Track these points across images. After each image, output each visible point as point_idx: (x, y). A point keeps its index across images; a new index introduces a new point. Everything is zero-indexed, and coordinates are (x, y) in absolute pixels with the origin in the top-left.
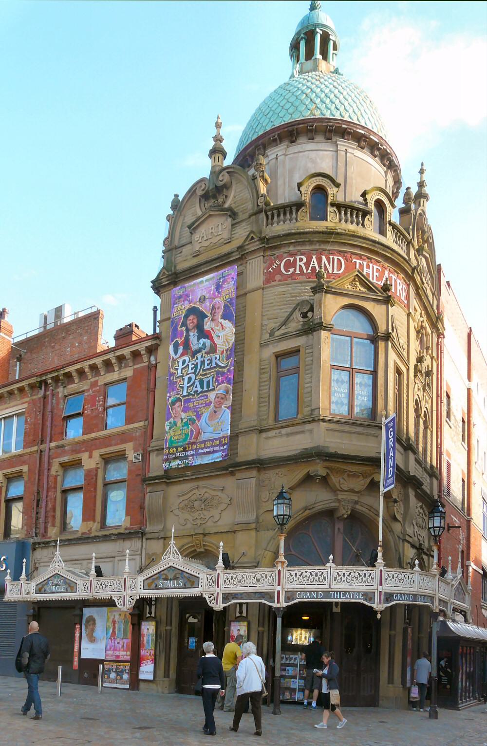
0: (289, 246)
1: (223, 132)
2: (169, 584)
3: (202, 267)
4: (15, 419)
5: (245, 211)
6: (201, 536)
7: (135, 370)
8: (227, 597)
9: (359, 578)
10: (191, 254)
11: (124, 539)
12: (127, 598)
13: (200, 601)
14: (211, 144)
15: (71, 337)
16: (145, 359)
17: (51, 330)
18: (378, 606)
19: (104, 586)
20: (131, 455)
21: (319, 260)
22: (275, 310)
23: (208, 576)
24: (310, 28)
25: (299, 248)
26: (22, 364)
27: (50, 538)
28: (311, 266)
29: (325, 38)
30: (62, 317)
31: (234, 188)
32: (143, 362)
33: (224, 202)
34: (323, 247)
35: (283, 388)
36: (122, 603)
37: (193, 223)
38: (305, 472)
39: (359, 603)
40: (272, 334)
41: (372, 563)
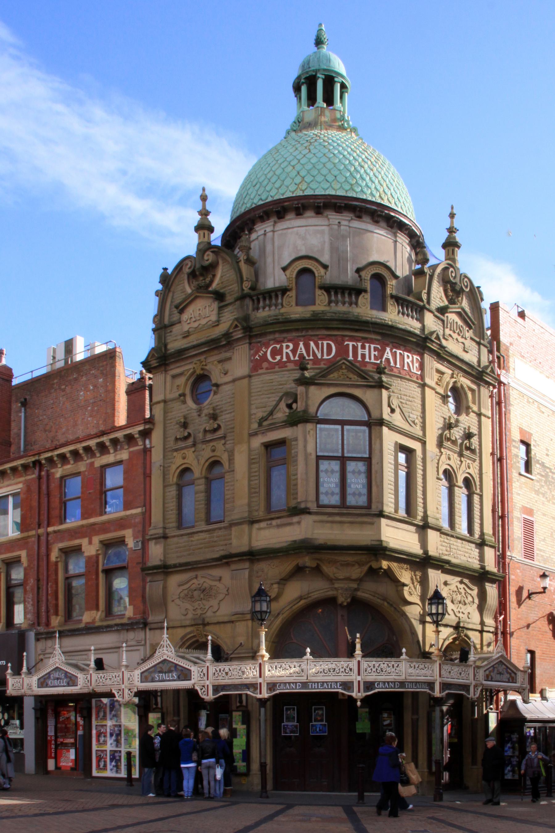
2: (164, 676)
3: (190, 351)
5: (232, 293)
6: (201, 626)
7: (130, 453)
8: (217, 689)
10: (181, 335)
11: (127, 630)
12: (126, 691)
13: (192, 693)
14: (196, 218)
15: (84, 379)
16: (140, 443)
18: (357, 694)
19: (104, 679)
20: (130, 542)
23: (199, 669)
25: (285, 335)
26: (28, 410)
27: (53, 628)
28: (298, 352)
29: (329, 81)
30: (74, 353)
33: (212, 282)
34: (310, 333)
37: (181, 304)
38: (294, 564)
40: (260, 424)
41: (351, 654)
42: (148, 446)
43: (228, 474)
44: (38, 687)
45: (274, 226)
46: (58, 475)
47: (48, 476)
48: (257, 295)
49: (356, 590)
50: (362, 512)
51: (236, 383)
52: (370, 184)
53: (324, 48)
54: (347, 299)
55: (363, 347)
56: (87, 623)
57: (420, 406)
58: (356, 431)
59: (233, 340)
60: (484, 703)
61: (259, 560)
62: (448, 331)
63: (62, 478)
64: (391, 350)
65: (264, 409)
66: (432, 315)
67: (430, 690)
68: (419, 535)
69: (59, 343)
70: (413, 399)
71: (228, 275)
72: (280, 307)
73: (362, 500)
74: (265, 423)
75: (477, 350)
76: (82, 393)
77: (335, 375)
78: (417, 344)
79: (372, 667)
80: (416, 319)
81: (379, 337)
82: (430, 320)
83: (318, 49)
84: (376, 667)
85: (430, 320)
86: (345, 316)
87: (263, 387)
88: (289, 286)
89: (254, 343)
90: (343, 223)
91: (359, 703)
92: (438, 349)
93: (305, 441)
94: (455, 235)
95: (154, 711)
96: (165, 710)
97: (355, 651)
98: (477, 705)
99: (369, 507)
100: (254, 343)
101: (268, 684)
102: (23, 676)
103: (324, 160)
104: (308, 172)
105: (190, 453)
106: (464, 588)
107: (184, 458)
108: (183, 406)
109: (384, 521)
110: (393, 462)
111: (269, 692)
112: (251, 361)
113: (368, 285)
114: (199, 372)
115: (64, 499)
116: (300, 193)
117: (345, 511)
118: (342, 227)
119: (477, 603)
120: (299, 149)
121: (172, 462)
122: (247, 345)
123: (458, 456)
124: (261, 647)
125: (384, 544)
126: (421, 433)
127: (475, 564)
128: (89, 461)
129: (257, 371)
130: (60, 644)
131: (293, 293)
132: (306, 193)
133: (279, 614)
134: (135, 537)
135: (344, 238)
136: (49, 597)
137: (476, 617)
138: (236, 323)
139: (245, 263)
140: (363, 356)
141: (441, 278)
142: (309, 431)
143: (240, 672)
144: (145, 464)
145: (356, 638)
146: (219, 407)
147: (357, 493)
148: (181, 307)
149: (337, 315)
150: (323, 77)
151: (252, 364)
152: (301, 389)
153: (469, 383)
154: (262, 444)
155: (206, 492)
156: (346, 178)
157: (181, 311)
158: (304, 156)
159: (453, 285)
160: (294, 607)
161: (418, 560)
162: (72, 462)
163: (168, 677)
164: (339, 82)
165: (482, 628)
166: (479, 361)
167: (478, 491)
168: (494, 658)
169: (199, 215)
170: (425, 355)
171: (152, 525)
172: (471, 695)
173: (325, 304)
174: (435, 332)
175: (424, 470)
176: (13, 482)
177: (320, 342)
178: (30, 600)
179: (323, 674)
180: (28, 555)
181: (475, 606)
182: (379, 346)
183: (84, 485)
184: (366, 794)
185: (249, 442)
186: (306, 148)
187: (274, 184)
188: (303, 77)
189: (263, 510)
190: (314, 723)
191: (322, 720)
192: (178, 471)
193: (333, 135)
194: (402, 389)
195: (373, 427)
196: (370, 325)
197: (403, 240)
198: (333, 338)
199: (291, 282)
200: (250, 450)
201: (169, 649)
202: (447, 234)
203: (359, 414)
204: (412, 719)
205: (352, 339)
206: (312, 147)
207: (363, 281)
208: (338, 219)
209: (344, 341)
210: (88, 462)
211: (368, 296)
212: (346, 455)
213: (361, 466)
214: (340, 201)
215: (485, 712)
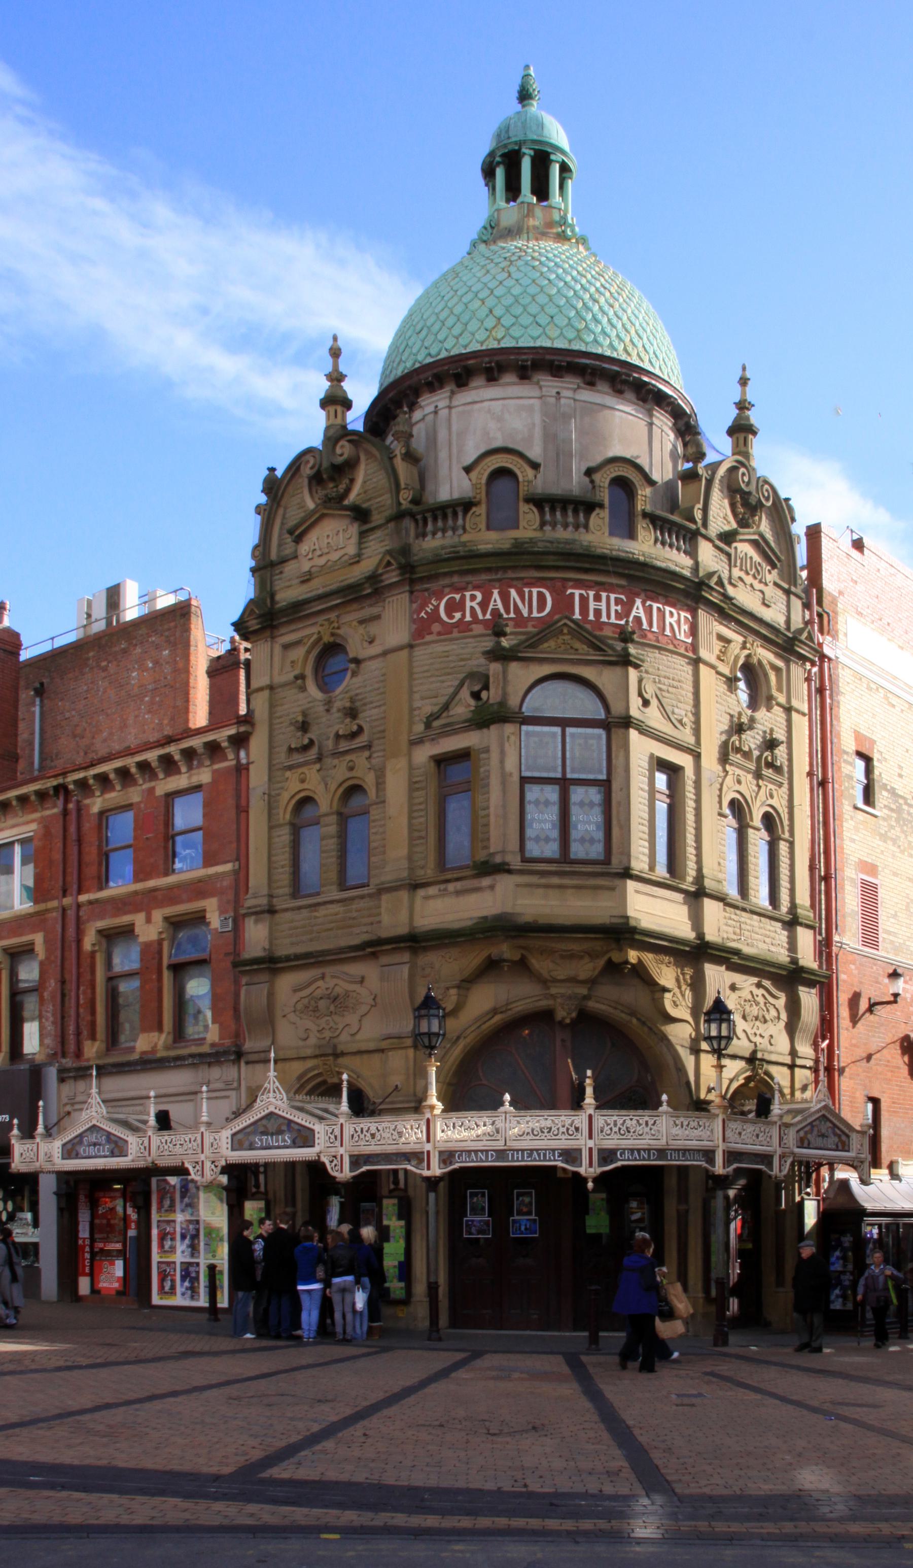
3: (313, 604)
6: (331, 1058)
7: (214, 772)
10: (298, 578)
11: (210, 1064)
12: (208, 1165)
13: (316, 1168)
14: (323, 386)
15: (138, 650)
16: (231, 756)
17: (99, 637)
18: (588, 1169)
19: (171, 1146)
20: (215, 920)
21: (505, 598)
22: (432, 683)
24: (510, 147)
25: (469, 578)
26: (46, 701)
27: (88, 1060)
28: (491, 607)
29: (542, 160)
30: (121, 608)
33: (348, 490)
34: (510, 574)
35: (450, 816)
36: (200, 1173)
37: (297, 526)
38: (485, 954)
40: (428, 725)
41: (577, 1103)
42: (244, 761)
43: (375, 807)
44: (63, 1158)
45: (451, 398)
46: (95, 809)
48: (423, 512)
49: (586, 998)
50: (596, 870)
51: (389, 656)
52: (608, 329)
53: (533, 105)
54: (571, 519)
55: (598, 598)
57: (690, 696)
60: (797, 1185)
61: (426, 949)
62: (736, 572)
63: (102, 813)
64: (643, 603)
65: (434, 700)
66: (710, 545)
67: (707, 1162)
69: (97, 591)
70: (679, 684)
72: (460, 531)
73: (596, 851)
74: (436, 724)
75: (785, 603)
76: (134, 674)
78: (686, 594)
79: (612, 1125)
80: (685, 552)
81: (623, 582)
82: (707, 554)
83: (523, 106)
84: (619, 1125)
85: (707, 554)
87: (432, 664)
88: (475, 498)
90: (565, 393)
92: (721, 601)
93: (502, 753)
94: (749, 413)
95: (253, 1197)
96: (271, 1196)
97: (583, 1099)
98: (784, 1188)
99: (607, 861)
100: (417, 591)
101: (441, 1153)
102: (38, 1140)
103: (533, 290)
104: (507, 311)
105: (312, 773)
106: (763, 995)
107: (303, 781)
108: (302, 695)
109: (631, 885)
110: (647, 788)
111: (442, 1165)
112: (414, 621)
113: (605, 496)
114: (327, 639)
115: (105, 849)
117: (567, 868)
118: (563, 401)
121: (282, 788)
122: (407, 594)
123: (754, 778)
124: (429, 1093)
125: (632, 923)
126: (691, 740)
127: (782, 955)
128: (146, 786)
129: (423, 638)
130: (99, 1087)
131: (482, 510)
132: (503, 345)
133: (458, 1038)
135: (566, 417)
136: (81, 1010)
138: (388, 558)
139: (403, 459)
140: (598, 612)
142: (508, 737)
143: (395, 1133)
148: (297, 533)
149: (555, 545)
150: (532, 153)
152: (495, 668)
153: (771, 657)
156: (569, 319)
157: (298, 539)
158: (501, 283)
159: (745, 495)
160: (484, 1027)
161: (687, 949)
162: (118, 787)
163: (277, 1141)
164: (558, 162)
165: (793, 1060)
166: (788, 622)
167: (786, 835)
168: (813, 1110)
169: (328, 380)
170: (700, 611)
171: (250, 891)
173: (534, 527)
174: (715, 573)
175: (698, 801)
176: (21, 820)
177: (526, 590)
178: (49, 1015)
179: (532, 1137)
180: (46, 941)
181: (782, 1024)
182: (623, 597)
183: (139, 826)
184: (601, 1334)
185: (409, 755)
186: (503, 269)
187: (450, 329)
188: (499, 153)
189: (432, 866)
191: (530, 1213)
192: (293, 802)
194: (661, 667)
196: (609, 562)
198: (549, 583)
199: (478, 491)
200: (411, 768)
201: (278, 1095)
202: (735, 412)
203: (591, 708)
204: (678, 1211)
205: (579, 584)
206: (512, 269)
207: (597, 488)
208: (557, 387)
209: (566, 589)
210: (144, 787)
211: (605, 514)
212: (569, 776)
213: (594, 795)
214: (560, 358)
215: (798, 1199)
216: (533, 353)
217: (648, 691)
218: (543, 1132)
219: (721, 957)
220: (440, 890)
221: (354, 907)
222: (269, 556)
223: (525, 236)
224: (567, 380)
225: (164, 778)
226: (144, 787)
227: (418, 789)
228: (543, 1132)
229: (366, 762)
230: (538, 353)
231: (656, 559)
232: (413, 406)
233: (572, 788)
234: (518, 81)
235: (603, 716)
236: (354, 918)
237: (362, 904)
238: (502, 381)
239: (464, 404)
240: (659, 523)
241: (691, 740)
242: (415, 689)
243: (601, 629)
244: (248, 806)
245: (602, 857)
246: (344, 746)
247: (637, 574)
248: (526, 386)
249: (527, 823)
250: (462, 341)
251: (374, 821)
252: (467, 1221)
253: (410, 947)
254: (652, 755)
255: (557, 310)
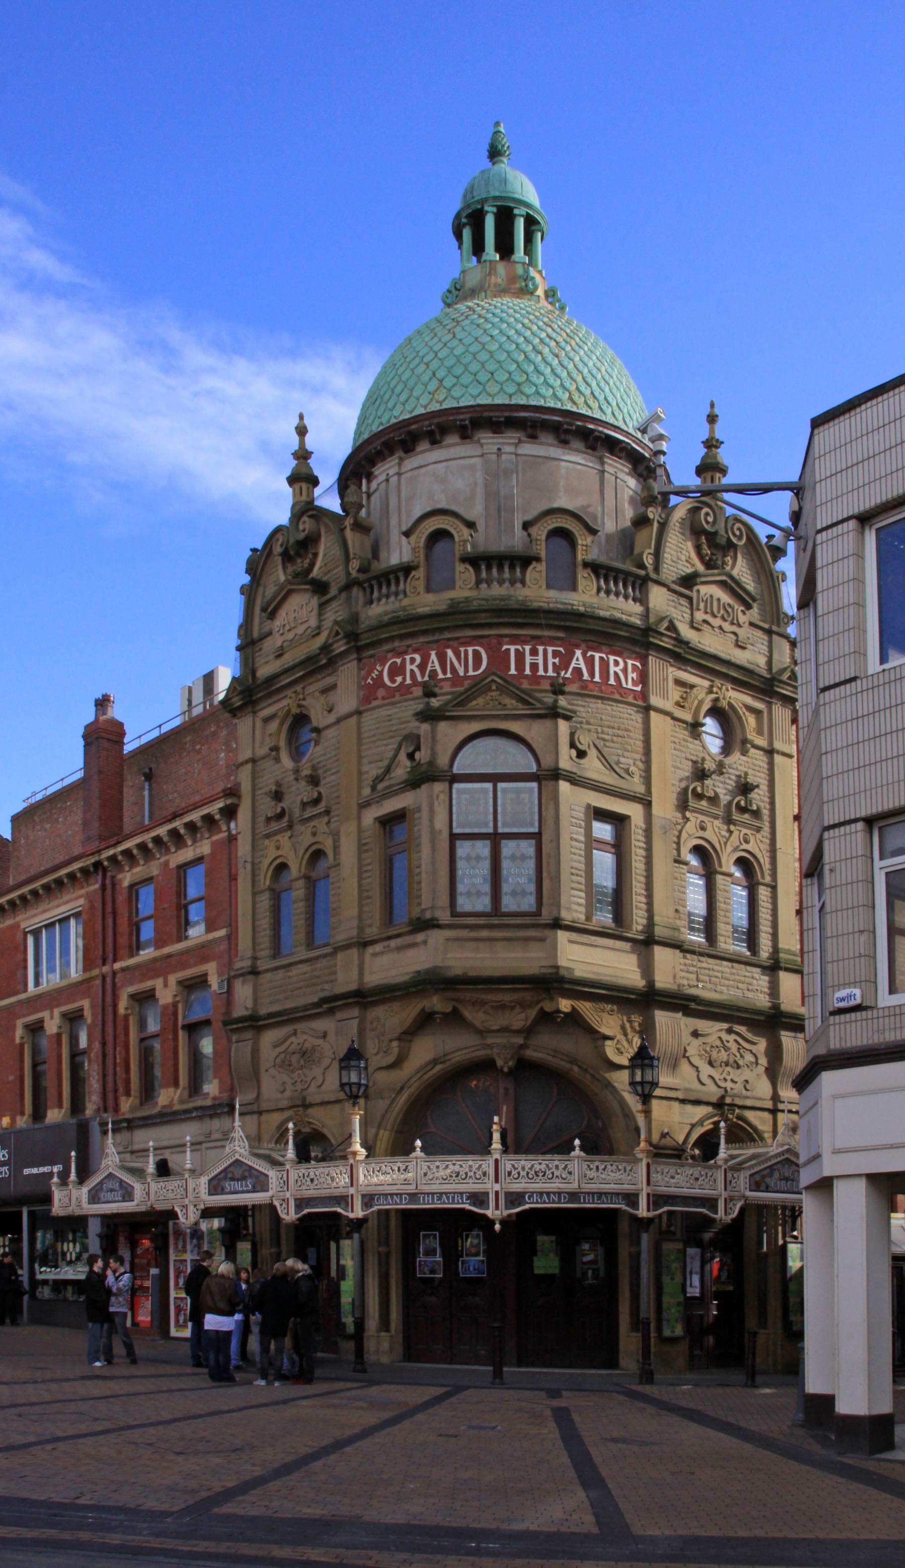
0: (393, 642)
1: (310, 442)
2: (237, 1186)
3: (282, 677)
4: (73, 922)
6: (301, 1109)
7: (213, 844)
9: (513, 1173)
12: (191, 1208)
15: (224, 733)
16: (224, 828)
20: (214, 982)
21: (442, 659)
22: (378, 747)
25: (409, 642)
26: (154, 785)
27: (123, 1114)
28: (429, 668)
29: (505, 217)
30: (215, 693)
31: (323, 539)
32: (221, 831)
33: (312, 565)
34: (447, 635)
39: (463, 1210)
40: (374, 788)
42: (234, 832)
43: (333, 870)
44: (89, 1203)
45: (400, 465)
46: (126, 883)
47: (114, 885)
48: (369, 580)
49: (522, 1047)
50: (524, 922)
51: (342, 723)
52: (551, 380)
53: (502, 162)
54: (507, 575)
55: (534, 652)
56: (164, 1107)
57: (640, 744)
58: (518, 791)
59: (336, 655)
60: (780, 1228)
61: (374, 1004)
62: (699, 616)
63: (131, 886)
64: (584, 654)
65: (380, 764)
66: (664, 590)
67: (628, 1205)
68: (639, 955)
69: (195, 677)
70: (625, 733)
71: (332, 552)
72: (401, 596)
73: (528, 903)
74: (380, 786)
75: (766, 643)
76: (222, 755)
77: (480, 701)
78: (633, 641)
79: (520, 1169)
80: (635, 600)
81: (561, 634)
82: (658, 598)
83: (494, 164)
84: (527, 1169)
85: (658, 598)
86: (503, 603)
87: (377, 728)
88: (413, 562)
89: (365, 658)
90: (507, 449)
91: (497, 1227)
92: (674, 646)
93: (432, 812)
94: (718, 450)
95: (244, 1238)
96: (258, 1238)
97: (490, 1144)
98: (766, 1231)
99: (538, 913)
100: (365, 658)
101: (363, 1196)
102: (71, 1187)
103: (474, 348)
104: (449, 372)
105: (284, 839)
106: (736, 1041)
107: (278, 848)
108: (277, 766)
109: (562, 936)
110: (582, 838)
112: (360, 687)
113: (542, 550)
114: (295, 710)
115: (135, 919)
116: (435, 407)
117: (496, 921)
118: (504, 457)
119: (766, 1064)
120: (439, 335)
121: (263, 856)
122: (355, 662)
123: (723, 823)
124: (353, 1140)
125: (562, 972)
126: (641, 789)
127: (762, 1001)
128: (163, 860)
129: (370, 703)
130: (113, 1138)
131: (420, 573)
132: (444, 406)
133: (402, 1088)
134: (220, 974)
135: (507, 473)
136: (118, 1069)
137: (763, 1088)
138: (337, 628)
139: (352, 530)
140: (534, 667)
141: (688, 525)
142: (438, 796)
143: (329, 1178)
144: (230, 860)
145: (493, 1123)
146: (322, 764)
147: (474, 891)
148: (269, 610)
149: (489, 603)
150: (495, 210)
151: (362, 693)
152: (424, 728)
153: (749, 700)
154: (376, 819)
155: (307, 900)
156: (510, 374)
157: (272, 615)
158: (445, 344)
159: (712, 537)
160: (426, 1077)
161: (633, 997)
162: (142, 862)
163: (242, 1186)
164: (522, 216)
165: (775, 1104)
166: (770, 663)
167: (768, 879)
168: (772, 1154)
169: (295, 459)
170: (650, 658)
171: (240, 954)
172: (720, 1214)
173: (469, 586)
174: (667, 616)
175: (649, 850)
176: (74, 895)
177: (462, 649)
178: (95, 1074)
179: (527, 1180)
180: (93, 1007)
181: (761, 1070)
182: (561, 649)
183: (158, 898)
184: (505, 1369)
185: (359, 818)
186: (449, 331)
187: (398, 396)
188: (464, 215)
189: (378, 925)
190: (465, 1258)
191: (477, 1254)
192: (272, 868)
193: (522, 306)
194: (604, 717)
195: (543, 783)
196: (542, 615)
197: (616, 467)
198: (484, 641)
199: (417, 555)
200: (360, 830)
201: (242, 1144)
204: (630, 1253)
205: (515, 639)
206: (458, 330)
207: (534, 543)
208: (498, 444)
209: (501, 645)
210: (162, 860)
211: (542, 567)
212: (500, 830)
213: (527, 848)
214: (497, 414)
215: (781, 1242)
216: (471, 412)
217: (582, 741)
218: (538, 1176)
219: (666, 1002)
220: (384, 947)
221: (318, 966)
222: (252, 634)
223: (483, 294)
224: (509, 435)
225: (176, 852)
226: (162, 860)
227: (366, 851)
228: (538, 1176)
229: (325, 827)
230: (475, 411)
231: (598, 608)
232: (370, 477)
233: (503, 842)
234: (488, 140)
235: (534, 768)
236: (319, 977)
237: (324, 963)
238: (444, 443)
239: (411, 470)
240: (603, 572)
241: (641, 789)
242: (364, 754)
243: (538, 683)
244: (237, 875)
245: (534, 909)
246: (310, 812)
247: (576, 625)
248: (468, 446)
249: (458, 879)
250: (409, 407)
251: (333, 883)
252: (420, 1261)
253: (357, 1003)
254: (589, 806)
255: (497, 366)
